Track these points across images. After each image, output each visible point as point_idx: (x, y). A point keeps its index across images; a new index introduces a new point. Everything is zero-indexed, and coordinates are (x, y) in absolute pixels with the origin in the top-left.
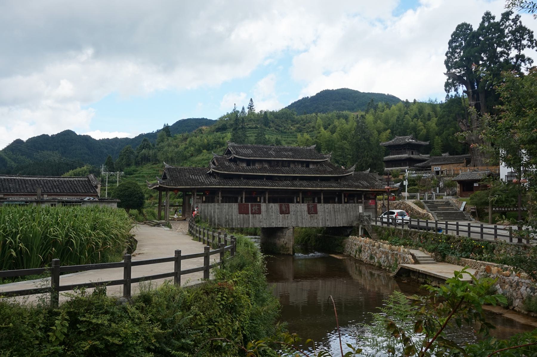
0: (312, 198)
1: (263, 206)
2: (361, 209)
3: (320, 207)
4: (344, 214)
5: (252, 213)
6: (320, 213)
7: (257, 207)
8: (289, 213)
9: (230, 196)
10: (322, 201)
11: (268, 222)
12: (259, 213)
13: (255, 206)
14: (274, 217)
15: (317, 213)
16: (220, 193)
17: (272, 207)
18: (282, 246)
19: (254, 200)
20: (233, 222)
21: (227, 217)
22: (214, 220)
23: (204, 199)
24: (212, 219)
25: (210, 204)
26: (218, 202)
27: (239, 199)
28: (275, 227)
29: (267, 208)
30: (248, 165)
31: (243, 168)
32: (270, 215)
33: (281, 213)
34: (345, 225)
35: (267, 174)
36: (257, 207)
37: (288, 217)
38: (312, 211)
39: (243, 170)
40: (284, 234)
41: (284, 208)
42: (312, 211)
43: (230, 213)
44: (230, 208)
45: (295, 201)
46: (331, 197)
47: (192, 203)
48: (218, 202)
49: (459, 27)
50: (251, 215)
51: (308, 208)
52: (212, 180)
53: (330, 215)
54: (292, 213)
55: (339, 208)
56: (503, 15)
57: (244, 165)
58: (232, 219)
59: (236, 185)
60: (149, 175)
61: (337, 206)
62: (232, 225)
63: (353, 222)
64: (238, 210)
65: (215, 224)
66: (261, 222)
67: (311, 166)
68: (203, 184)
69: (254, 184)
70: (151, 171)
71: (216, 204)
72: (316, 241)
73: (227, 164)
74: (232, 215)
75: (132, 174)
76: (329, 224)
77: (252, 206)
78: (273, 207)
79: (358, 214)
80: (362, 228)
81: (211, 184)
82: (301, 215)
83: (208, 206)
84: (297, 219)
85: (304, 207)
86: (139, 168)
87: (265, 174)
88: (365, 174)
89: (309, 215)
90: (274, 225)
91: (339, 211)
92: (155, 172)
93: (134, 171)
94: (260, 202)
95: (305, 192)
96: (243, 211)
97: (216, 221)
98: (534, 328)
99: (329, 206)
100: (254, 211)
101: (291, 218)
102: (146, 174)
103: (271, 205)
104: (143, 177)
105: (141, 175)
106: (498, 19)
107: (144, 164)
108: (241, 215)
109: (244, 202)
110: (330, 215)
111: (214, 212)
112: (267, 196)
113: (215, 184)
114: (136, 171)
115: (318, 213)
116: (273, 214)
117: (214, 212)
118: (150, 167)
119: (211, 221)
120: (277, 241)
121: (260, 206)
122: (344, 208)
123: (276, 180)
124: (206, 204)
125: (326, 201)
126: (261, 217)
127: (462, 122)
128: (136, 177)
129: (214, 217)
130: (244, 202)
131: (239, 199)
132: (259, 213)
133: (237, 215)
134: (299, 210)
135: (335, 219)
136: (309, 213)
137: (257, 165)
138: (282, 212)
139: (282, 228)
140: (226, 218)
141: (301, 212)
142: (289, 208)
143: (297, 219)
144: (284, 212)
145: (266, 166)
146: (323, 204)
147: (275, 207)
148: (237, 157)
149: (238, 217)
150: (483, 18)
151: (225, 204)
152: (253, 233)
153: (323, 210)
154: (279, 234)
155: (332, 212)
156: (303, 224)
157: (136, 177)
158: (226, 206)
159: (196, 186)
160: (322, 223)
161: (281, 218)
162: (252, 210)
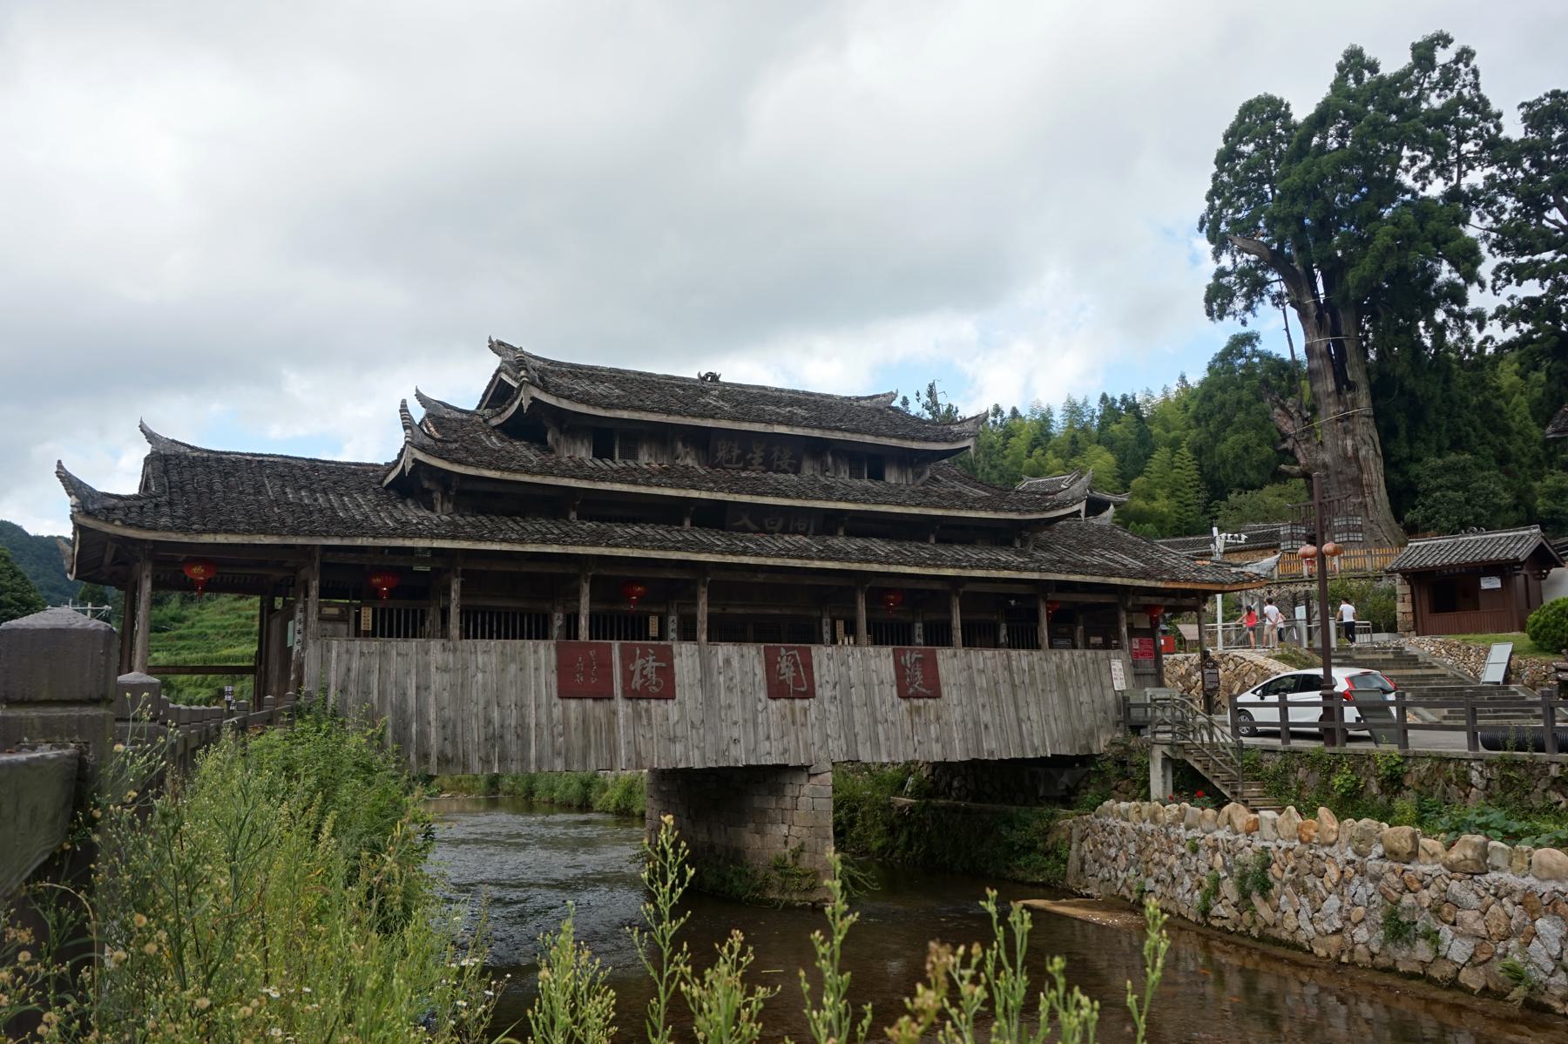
0: (910, 619)
1: (686, 658)
2: (1119, 674)
3: (951, 662)
4: (1055, 698)
5: (631, 695)
6: (950, 693)
7: (652, 664)
8: (809, 694)
9: (509, 602)
10: (958, 635)
11: (710, 738)
12: (667, 693)
13: (644, 655)
14: (737, 714)
15: (936, 694)
16: (456, 586)
17: (727, 662)
18: (780, 866)
19: (633, 628)
20: (525, 746)
21: (496, 715)
22: (423, 734)
23: (367, 622)
24: (407, 727)
25: (397, 646)
26: (445, 634)
27: (558, 621)
28: (748, 768)
29: (706, 670)
30: (602, 451)
31: (580, 465)
32: (715, 705)
33: (773, 696)
34: (1064, 750)
35: (704, 495)
36: (652, 664)
37: (805, 711)
38: (918, 685)
39: (577, 470)
40: (788, 802)
41: (788, 673)
42: (918, 685)
43: (510, 697)
44: (513, 668)
45: (827, 637)
46: (1006, 618)
47: (293, 640)
48: (445, 634)
49: (1248, 109)
50: (622, 707)
51: (900, 668)
52: (413, 514)
53: (1001, 705)
54: (824, 692)
55: (1031, 668)
56: (1415, 48)
57: (584, 452)
58: (522, 726)
59: (544, 542)
60: (223, 632)
61: (1022, 659)
62: (524, 760)
63: (1091, 734)
64: (554, 679)
65: (424, 757)
66: (673, 740)
67: (892, 477)
68: (359, 528)
69: (631, 542)
70: (231, 619)
71: (435, 645)
72: (892, 830)
73: (494, 442)
74: (520, 706)
75: (165, 630)
76: (995, 747)
77: (627, 658)
78: (735, 662)
79: (1110, 696)
80: (1166, 760)
81: (404, 530)
82: (869, 703)
83: (384, 654)
84: (847, 723)
85: (881, 661)
86: (191, 611)
87: (694, 494)
88: (1100, 529)
89: (905, 705)
90: (740, 756)
91: (1033, 683)
92: (243, 621)
93: (173, 619)
94: (662, 635)
95: (879, 588)
96: (581, 681)
97: (433, 733)
98: (11, 703)
99: (986, 659)
100: (637, 683)
101: (823, 718)
102: (214, 627)
103: (724, 650)
104: (203, 636)
105: (196, 630)
106: (1388, 69)
107: (209, 599)
108: (573, 704)
109: (584, 633)
110: (1001, 705)
111: (422, 688)
112: (702, 611)
113: (428, 532)
114: (181, 620)
115: (945, 690)
116: (736, 699)
117: (422, 688)
118: (226, 607)
119: (401, 738)
120: (751, 840)
121: (666, 656)
122: (1050, 667)
123: (745, 530)
124: (375, 644)
125: (979, 636)
126: (674, 715)
127: (1283, 407)
128: (180, 637)
129: (421, 713)
130: (584, 633)
131: (558, 621)
132: (667, 693)
133: (550, 707)
134: (854, 670)
135: (1019, 721)
136: (903, 695)
137: (645, 459)
138: (777, 690)
139: (782, 769)
140: (489, 722)
141: (867, 686)
142: (808, 667)
143: (847, 723)
144: (790, 687)
145: (690, 462)
146: (961, 652)
147: (744, 662)
148: (551, 400)
149: (557, 712)
150: (1340, 68)
151: (481, 644)
152: (576, 802)
153: (962, 678)
154: (757, 802)
155: (1004, 689)
156: (876, 745)
157: (180, 637)
158: (486, 654)
159: (312, 534)
160: (965, 739)
161: (774, 718)
162: (627, 676)
